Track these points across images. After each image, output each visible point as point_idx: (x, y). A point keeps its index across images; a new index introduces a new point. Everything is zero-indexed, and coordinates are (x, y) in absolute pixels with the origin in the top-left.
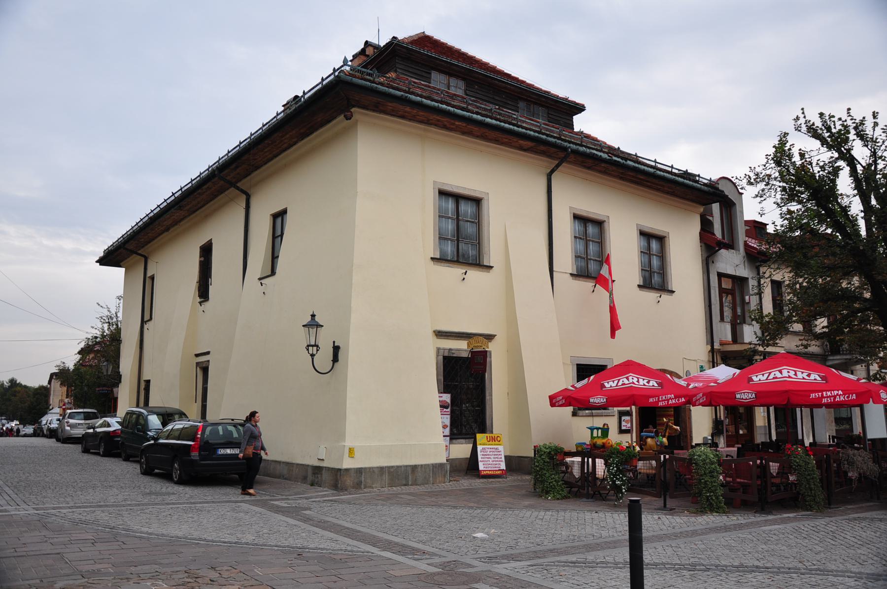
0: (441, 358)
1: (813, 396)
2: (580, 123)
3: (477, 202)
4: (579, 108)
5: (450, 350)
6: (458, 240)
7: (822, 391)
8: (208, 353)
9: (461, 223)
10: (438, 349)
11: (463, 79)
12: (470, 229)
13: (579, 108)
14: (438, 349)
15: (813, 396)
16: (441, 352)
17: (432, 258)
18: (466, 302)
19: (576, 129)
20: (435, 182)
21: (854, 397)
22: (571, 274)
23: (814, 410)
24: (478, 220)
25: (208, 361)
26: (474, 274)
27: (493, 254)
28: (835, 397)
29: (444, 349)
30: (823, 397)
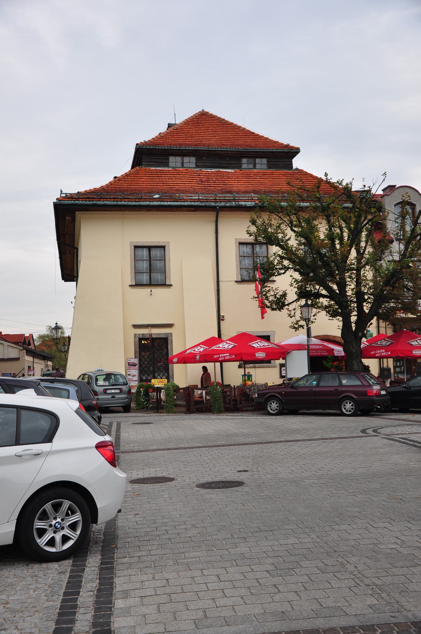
0: (137, 339)
1: (215, 357)
2: (297, 163)
3: (163, 247)
4: (295, 152)
5: (143, 334)
6: (150, 272)
7: (219, 354)
8: (170, 326)
9: (152, 262)
10: (135, 335)
11: (194, 156)
12: (158, 265)
13: (295, 152)
14: (135, 335)
15: (215, 357)
16: (137, 336)
17: (130, 286)
18: (152, 308)
19: (294, 167)
20: (131, 242)
21: (390, 353)
22: (236, 282)
23: (224, 363)
24: (163, 259)
25: (171, 334)
26: (158, 291)
27: (173, 277)
28: (225, 357)
29: (139, 334)
30: (219, 357)
